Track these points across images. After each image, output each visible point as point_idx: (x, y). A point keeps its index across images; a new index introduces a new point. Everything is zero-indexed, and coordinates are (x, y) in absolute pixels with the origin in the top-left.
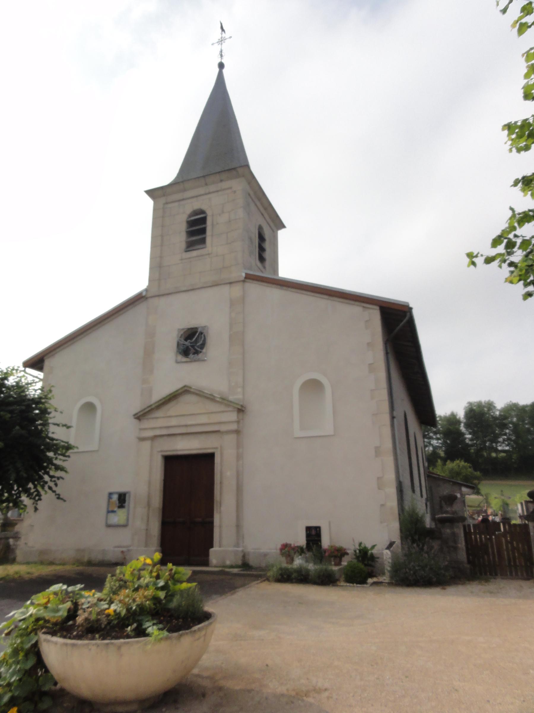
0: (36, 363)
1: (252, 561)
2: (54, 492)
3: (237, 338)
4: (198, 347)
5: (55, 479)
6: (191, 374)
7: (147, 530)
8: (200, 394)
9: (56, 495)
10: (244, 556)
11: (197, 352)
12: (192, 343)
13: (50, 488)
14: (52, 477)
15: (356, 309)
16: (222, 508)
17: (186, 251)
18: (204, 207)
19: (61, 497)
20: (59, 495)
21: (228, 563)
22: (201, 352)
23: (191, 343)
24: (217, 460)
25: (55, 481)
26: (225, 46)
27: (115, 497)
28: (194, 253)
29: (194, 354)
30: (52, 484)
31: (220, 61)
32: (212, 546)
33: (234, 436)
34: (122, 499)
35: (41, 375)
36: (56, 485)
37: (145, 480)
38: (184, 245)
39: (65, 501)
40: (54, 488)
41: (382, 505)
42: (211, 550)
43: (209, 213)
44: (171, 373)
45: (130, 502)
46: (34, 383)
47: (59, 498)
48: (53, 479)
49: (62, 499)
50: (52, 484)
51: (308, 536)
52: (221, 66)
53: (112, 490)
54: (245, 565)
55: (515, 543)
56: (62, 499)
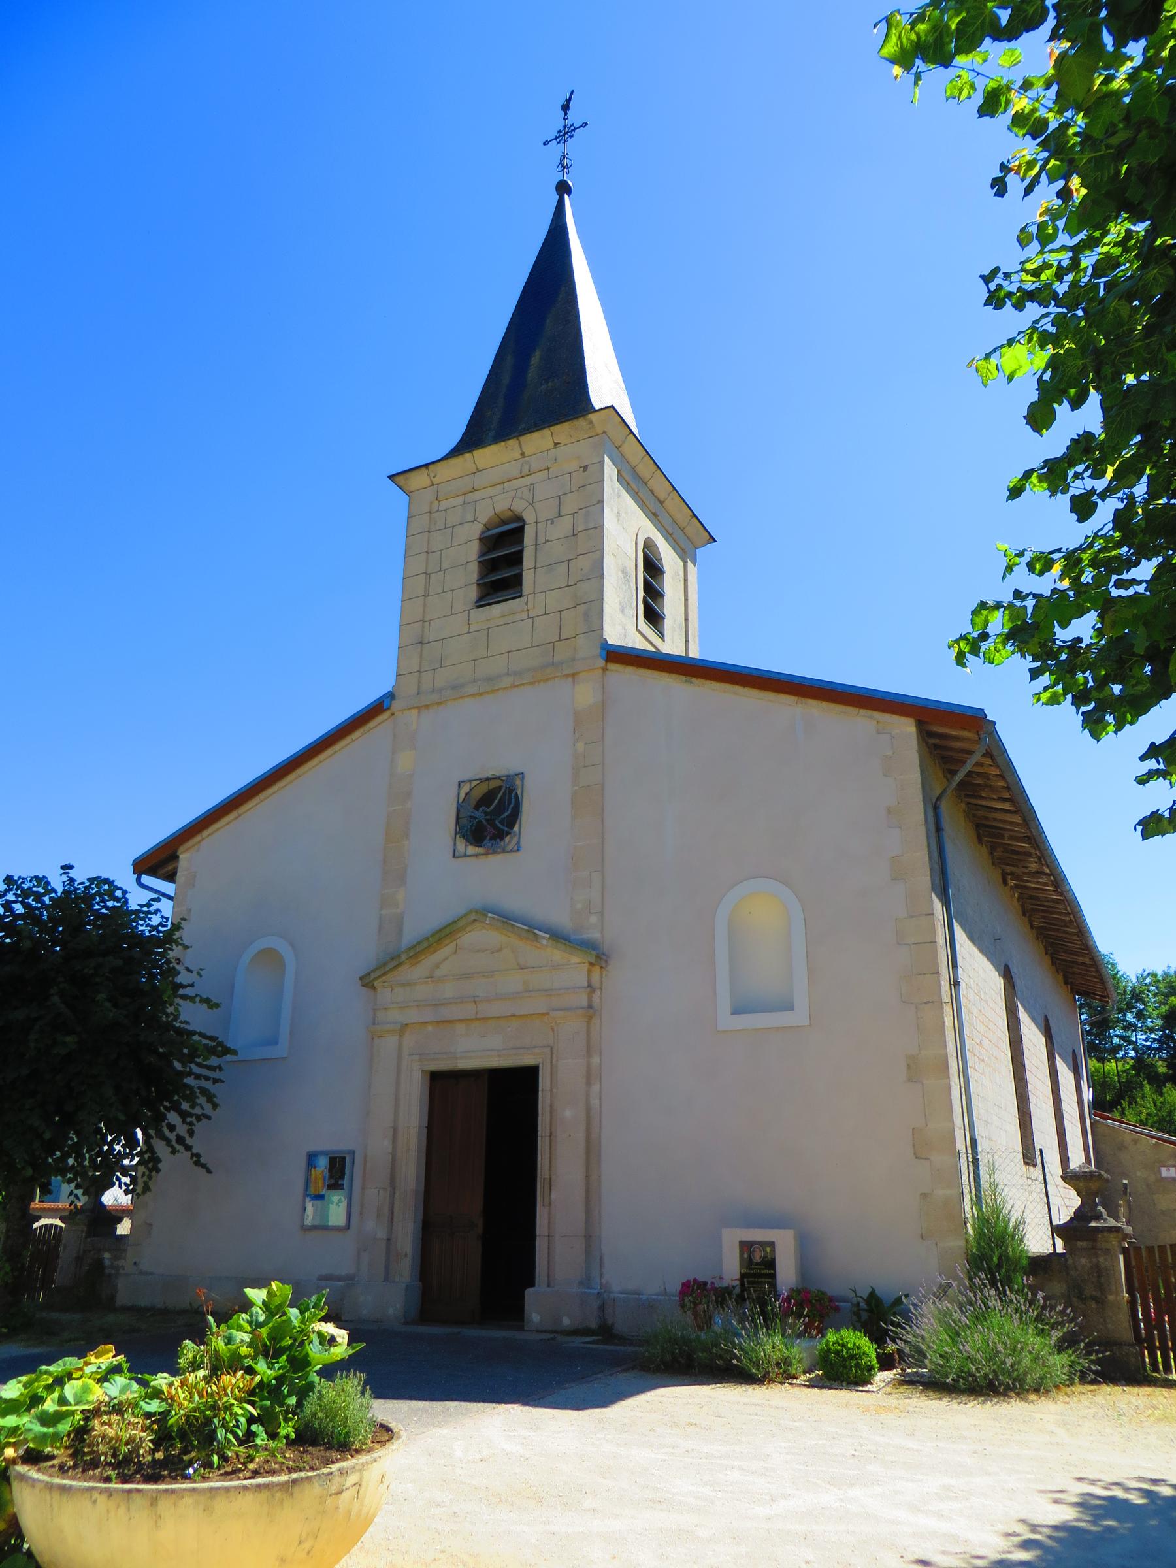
0: (159, 862)
1: (621, 1323)
2: (188, 1148)
3: (589, 800)
4: (502, 822)
5: (193, 1119)
6: (491, 876)
7: (388, 1240)
8: (506, 919)
9: (193, 1156)
10: (602, 1308)
11: (500, 835)
12: (490, 816)
13: (180, 1140)
14: (184, 1115)
15: (863, 722)
16: (553, 1196)
17: (478, 607)
18: (519, 506)
19: (203, 1160)
20: (198, 1156)
21: (566, 1321)
22: (508, 833)
23: (486, 813)
24: (544, 1082)
25: (191, 1124)
26: (571, 146)
27: (323, 1163)
28: (496, 610)
29: (493, 838)
30: (182, 1130)
31: (559, 177)
32: (532, 1284)
33: (585, 1003)
34: (338, 1170)
35: (168, 888)
36: (191, 1133)
37: (386, 1124)
38: (473, 593)
39: (209, 1171)
40: (189, 1141)
41: (924, 1196)
42: (529, 1292)
43: (529, 517)
44: (447, 876)
45: (356, 1174)
46: (153, 902)
47: (197, 1163)
48: (189, 1120)
49: (204, 1166)
50: (182, 1130)
51: (747, 1262)
52: (563, 188)
53: (313, 1148)
54: (606, 1332)
55: (138, 1131)
56: (204, 1166)
